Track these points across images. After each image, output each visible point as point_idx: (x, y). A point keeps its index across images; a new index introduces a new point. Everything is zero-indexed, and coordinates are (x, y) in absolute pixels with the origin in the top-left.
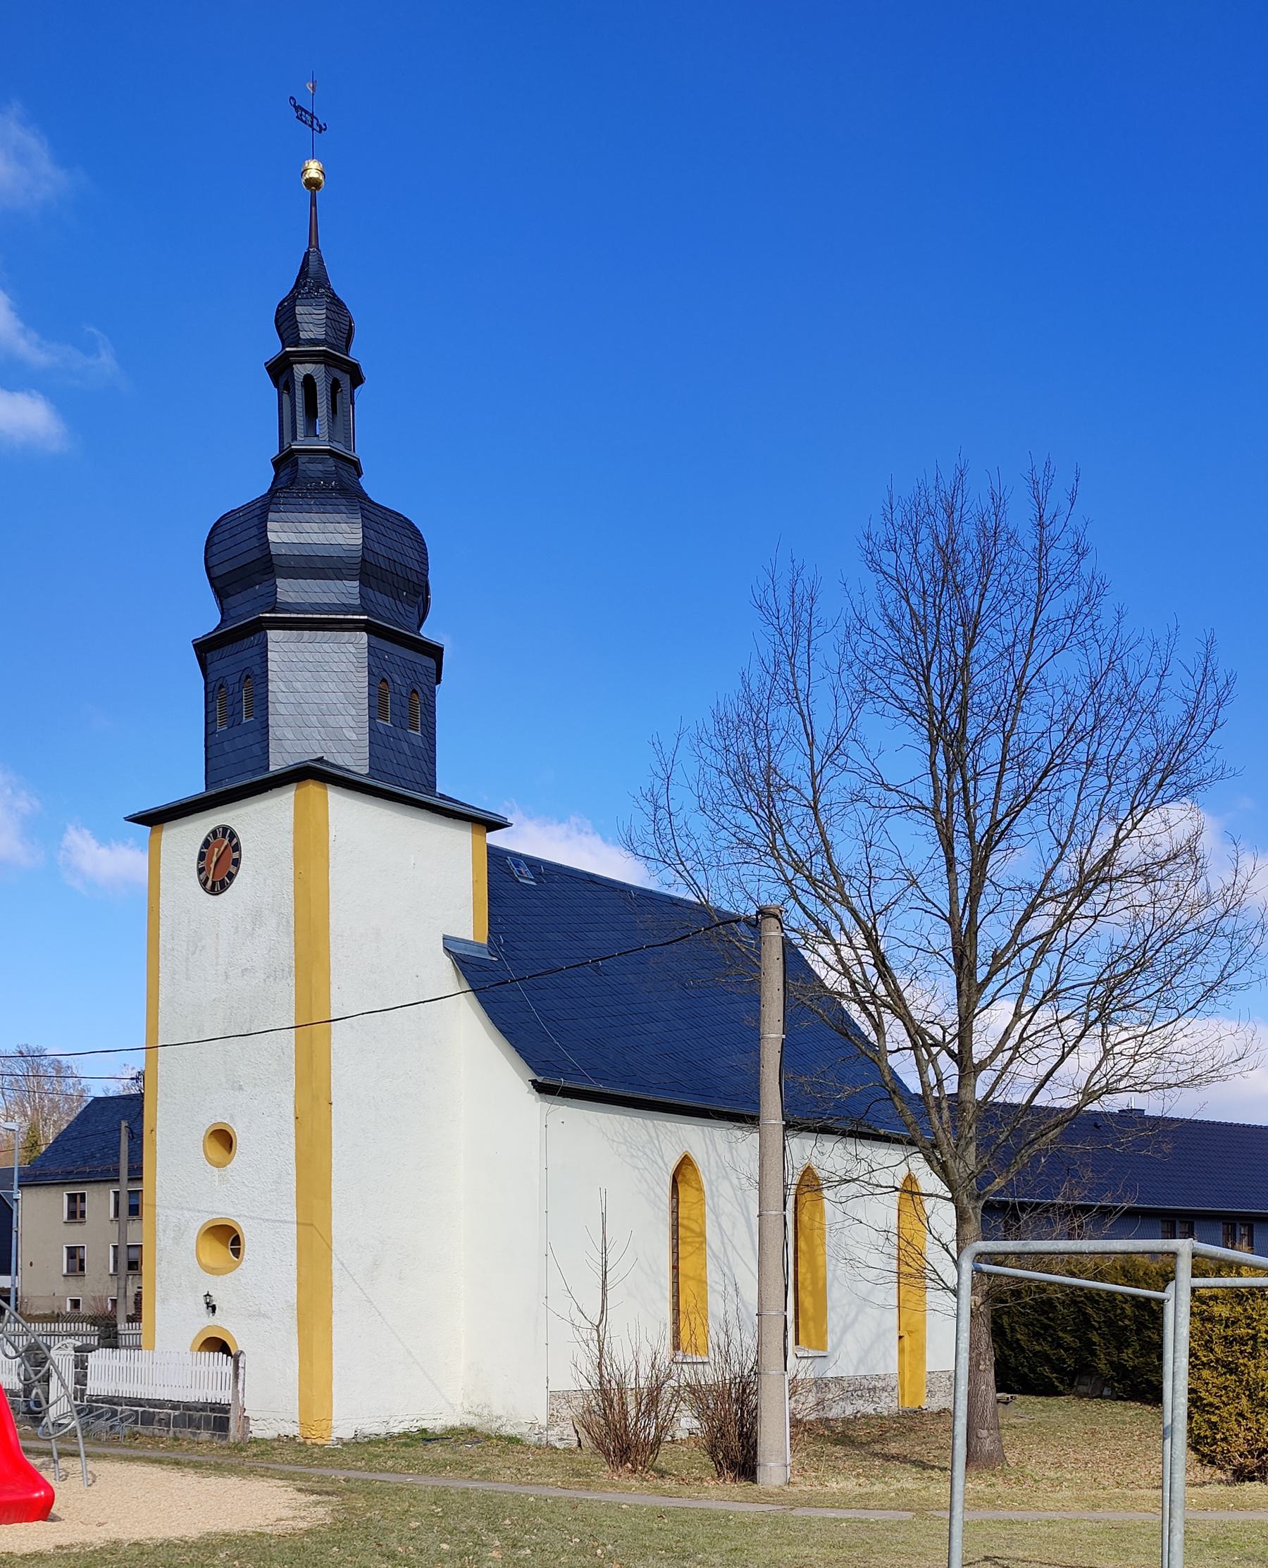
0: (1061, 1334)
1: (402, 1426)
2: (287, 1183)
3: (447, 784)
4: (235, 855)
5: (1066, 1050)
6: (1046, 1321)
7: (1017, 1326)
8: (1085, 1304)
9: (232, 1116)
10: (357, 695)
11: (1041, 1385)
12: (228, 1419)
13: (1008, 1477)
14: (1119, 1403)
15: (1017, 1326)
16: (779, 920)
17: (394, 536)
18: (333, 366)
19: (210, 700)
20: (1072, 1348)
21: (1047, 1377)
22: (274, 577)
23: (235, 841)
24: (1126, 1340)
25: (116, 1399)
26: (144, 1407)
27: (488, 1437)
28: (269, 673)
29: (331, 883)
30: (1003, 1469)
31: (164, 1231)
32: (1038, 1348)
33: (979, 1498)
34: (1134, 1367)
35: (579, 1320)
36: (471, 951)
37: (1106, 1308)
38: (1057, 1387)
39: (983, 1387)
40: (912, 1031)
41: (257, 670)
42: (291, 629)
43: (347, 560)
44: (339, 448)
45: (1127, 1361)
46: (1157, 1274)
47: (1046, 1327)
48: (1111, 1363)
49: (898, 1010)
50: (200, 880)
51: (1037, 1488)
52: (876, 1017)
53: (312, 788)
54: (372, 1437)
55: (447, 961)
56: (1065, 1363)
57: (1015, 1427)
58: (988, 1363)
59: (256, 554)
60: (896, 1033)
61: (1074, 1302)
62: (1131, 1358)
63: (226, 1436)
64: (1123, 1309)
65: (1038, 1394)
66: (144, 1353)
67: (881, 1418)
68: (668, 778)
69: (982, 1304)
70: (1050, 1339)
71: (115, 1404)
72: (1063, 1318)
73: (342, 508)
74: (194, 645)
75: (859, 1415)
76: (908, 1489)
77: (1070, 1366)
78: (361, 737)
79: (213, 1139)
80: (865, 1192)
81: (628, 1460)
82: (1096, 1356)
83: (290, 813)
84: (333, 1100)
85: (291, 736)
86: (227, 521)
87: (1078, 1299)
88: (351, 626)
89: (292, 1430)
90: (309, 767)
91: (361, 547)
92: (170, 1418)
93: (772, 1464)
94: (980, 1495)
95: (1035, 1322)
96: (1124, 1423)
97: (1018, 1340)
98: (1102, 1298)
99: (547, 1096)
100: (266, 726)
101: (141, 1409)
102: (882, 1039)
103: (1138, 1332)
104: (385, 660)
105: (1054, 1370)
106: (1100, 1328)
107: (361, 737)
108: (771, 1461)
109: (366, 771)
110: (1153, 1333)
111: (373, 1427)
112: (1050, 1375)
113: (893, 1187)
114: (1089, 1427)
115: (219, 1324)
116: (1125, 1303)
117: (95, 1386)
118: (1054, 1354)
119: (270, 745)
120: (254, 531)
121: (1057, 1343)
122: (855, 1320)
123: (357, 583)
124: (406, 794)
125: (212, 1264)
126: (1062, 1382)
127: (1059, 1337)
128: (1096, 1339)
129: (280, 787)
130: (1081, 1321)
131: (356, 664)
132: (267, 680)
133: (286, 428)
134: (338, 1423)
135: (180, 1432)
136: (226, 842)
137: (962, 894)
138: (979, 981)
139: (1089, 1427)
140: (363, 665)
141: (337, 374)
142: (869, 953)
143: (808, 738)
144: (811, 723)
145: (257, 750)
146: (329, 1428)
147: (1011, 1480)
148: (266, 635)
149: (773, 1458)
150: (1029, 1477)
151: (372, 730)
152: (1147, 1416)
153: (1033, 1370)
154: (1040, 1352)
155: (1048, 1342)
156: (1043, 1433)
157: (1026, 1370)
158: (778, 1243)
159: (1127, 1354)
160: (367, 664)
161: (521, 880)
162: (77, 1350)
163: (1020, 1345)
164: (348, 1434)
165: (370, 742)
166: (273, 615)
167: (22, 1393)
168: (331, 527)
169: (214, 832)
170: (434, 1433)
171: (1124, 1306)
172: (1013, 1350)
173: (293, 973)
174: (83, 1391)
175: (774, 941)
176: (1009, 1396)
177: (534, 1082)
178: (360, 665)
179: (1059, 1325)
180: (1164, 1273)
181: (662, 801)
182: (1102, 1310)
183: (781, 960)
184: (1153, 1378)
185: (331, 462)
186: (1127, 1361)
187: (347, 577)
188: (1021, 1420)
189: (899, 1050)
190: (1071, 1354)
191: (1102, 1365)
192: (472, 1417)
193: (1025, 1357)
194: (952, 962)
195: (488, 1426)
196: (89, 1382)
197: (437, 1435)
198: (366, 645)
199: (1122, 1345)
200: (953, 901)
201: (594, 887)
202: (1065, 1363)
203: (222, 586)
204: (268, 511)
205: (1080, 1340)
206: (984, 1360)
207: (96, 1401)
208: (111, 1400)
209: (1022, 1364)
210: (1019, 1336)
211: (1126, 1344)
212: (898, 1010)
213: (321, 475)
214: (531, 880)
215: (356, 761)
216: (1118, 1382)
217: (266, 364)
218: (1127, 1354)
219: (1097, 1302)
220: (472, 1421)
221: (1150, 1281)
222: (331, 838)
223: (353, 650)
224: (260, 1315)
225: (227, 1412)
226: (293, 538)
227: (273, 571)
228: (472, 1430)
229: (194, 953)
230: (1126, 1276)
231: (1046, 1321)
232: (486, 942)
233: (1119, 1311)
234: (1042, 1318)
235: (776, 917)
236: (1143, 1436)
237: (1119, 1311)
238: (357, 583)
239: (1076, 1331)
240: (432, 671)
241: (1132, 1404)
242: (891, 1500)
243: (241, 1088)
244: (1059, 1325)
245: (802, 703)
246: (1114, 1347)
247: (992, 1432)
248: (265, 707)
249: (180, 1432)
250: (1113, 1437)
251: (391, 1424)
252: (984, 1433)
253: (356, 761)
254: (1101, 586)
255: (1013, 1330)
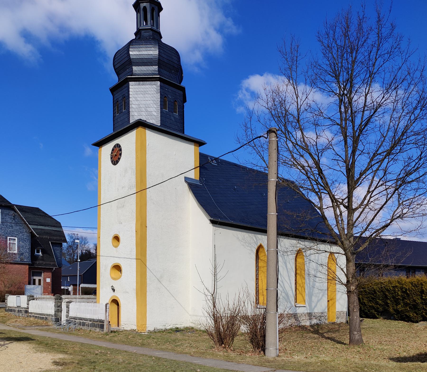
0: (378, 300)
1: (170, 326)
2: (133, 252)
3: (188, 133)
4: (120, 152)
5: (388, 199)
6: (373, 297)
7: (364, 298)
8: (386, 292)
9: (119, 232)
10: (157, 101)
11: (371, 315)
12: (104, 325)
13: (364, 348)
14: (396, 321)
15: (364, 298)
16: (276, 134)
17: (169, 52)
18: (152, 3)
19: (114, 106)
20: (381, 305)
21: (373, 313)
22: (132, 66)
23: (120, 148)
24: (399, 303)
25: (76, 318)
26: (83, 320)
27: (197, 330)
28: (130, 95)
29: (147, 158)
30: (362, 345)
31: (102, 267)
32: (371, 305)
33: (357, 367)
34: (402, 310)
35: (207, 293)
36: (194, 182)
37: (392, 293)
38: (377, 316)
39: (355, 317)
40: (331, 196)
41: (127, 95)
42: (136, 81)
43: (154, 59)
44: (155, 28)
45: (399, 309)
46: (409, 282)
47: (373, 299)
48: (394, 309)
49: (327, 189)
50: (111, 161)
51: (375, 353)
52: (319, 195)
53: (140, 129)
54: (160, 330)
55: (186, 185)
56: (379, 309)
57: (364, 328)
58: (357, 309)
59: (127, 59)
60: (327, 201)
61: (382, 291)
62: (400, 308)
63: (103, 330)
64: (398, 293)
65: (371, 318)
66: (97, 304)
67: (322, 325)
68: (251, 118)
69: (355, 289)
70: (374, 302)
71: (76, 319)
72: (379, 296)
73: (153, 43)
74: (110, 90)
75: (315, 324)
76: (326, 361)
77: (381, 310)
78: (158, 114)
79: (115, 239)
80: (315, 253)
81: (223, 343)
82: (389, 307)
83: (135, 137)
84: (147, 226)
85: (136, 114)
86: (117, 54)
87: (383, 290)
88: (155, 79)
89: (135, 328)
90: (139, 121)
91: (158, 55)
92: (89, 324)
93: (271, 349)
94: (357, 365)
95: (370, 297)
96: (399, 328)
97: (365, 302)
98: (391, 290)
99: (215, 225)
100: (129, 112)
101: (82, 321)
102: (321, 201)
103: (403, 300)
104: (166, 90)
105: (376, 311)
106: (390, 299)
107: (158, 114)
108: (271, 347)
109: (159, 125)
110: (408, 300)
111: (160, 327)
112: (374, 312)
113: (325, 251)
114: (388, 329)
115: (116, 295)
116: (399, 291)
117: (71, 314)
118: (376, 306)
119: (130, 118)
120: (126, 52)
121: (377, 303)
122: (321, 298)
123: (157, 67)
124: (172, 132)
125: (114, 277)
126: (378, 315)
127: (377, 302)
128: (389, 302)
129: (132, 130)
130: (384, 297)
131: (156, 91)
132: (129, 98)
133: (139, 23)
134: (149, 326)
135: (92, 329)
136: (118, 149)
137: (350, 151)
138: (355, 179)
139: (388, 329)
140: (158, 92)
141: (153, 6)
142: (316, 169)
143: (296, 96)
144: (297, 90)
145: (126, 119)
146: (145, 327)
147: (365, 349)
148: (129, 83)
149: (272, 346)
150: (372, 348)
151: (161, 112)
152: (406, 326)
153: (369, 312)
154: (371, 306)
155: (374, 303)
156: (373, 331)
157: (367, 311)
158: (275, 261)
159: (399, 306)
160: (160, 91)
161: (212, 164)
162: (67, 303)
163: (365, 304)
164: (152, 329)
165: (161, 116)
166: (131, 77)
167: (54, 316)
168: (149, 49)
169: (115, 146)
170: (181, 329)
171: (398, 292)
172: (363, 305)
173: (135, 187)
174: (68, 315)
175: (273, 142)
176: (362, 319)
177: (210, 220)
178: (158, 92)
179: (377, 298)
180: (411, 282)
181: (249, 126)
182: (391, 293)
183: (276, 150)
184: (407, 314)
185: (151, 32)
186: (399, 309)
187: (154, 65)
188: (366, 326)
189: (328, 208)
190: (381, 306)
191: (391, 310)
192: (193, 324)
193: (366, 307)
194: (346, 174)
195: (197, 327)
196: (70, 312)
197: (181, 329)
198: (159, 85)
199: (397, 303)
200: (346, 156)
201: (235, 167)
202: (379, 309)
203: (118, 71)
204: (130, 45)
205: (384, 302)
206: (356, 308)
207: (71, 318)
208: (75, 318)
209: (365, 309)
210: (365, 301)
211: (399, 304)
212: (327, 189)
213: (148, 36)
214: (216, 164)
215: (156, 120)
216: (396, 315)
217: (133, 5)
218: (399, 306)
219: (390, 291)
220: (192, 325)
221: (407, 285)
222: (147, 144)
223: (156, 87)
224: (127, 292)
225: (104, 322)
226: (137, 53)
227: (132, 64)
228: (193, 328)
229: (110, 183)
230: (399, 283)
231: (373, 297)
232: (198, 179)
233: (396, 294)
234: (372, 296)
235: (274, 132)
236: (406, 332)
237: (396, 294)
238: (157, 67)
239: (382, 300)
240: (181, 95)
241: (401, 322)
242: (318, 366)
243: (121, 223)
244: (377, 298)
245: (294, 85)
246: (395, 304)
247: (358, 332)
248: (129, 106)
249: (92, 329)
250: (397, 332)
251: (166, 326)
252: (356, 333)
253: (156, 120)
254: (401, 37)
255: (363, 299)
